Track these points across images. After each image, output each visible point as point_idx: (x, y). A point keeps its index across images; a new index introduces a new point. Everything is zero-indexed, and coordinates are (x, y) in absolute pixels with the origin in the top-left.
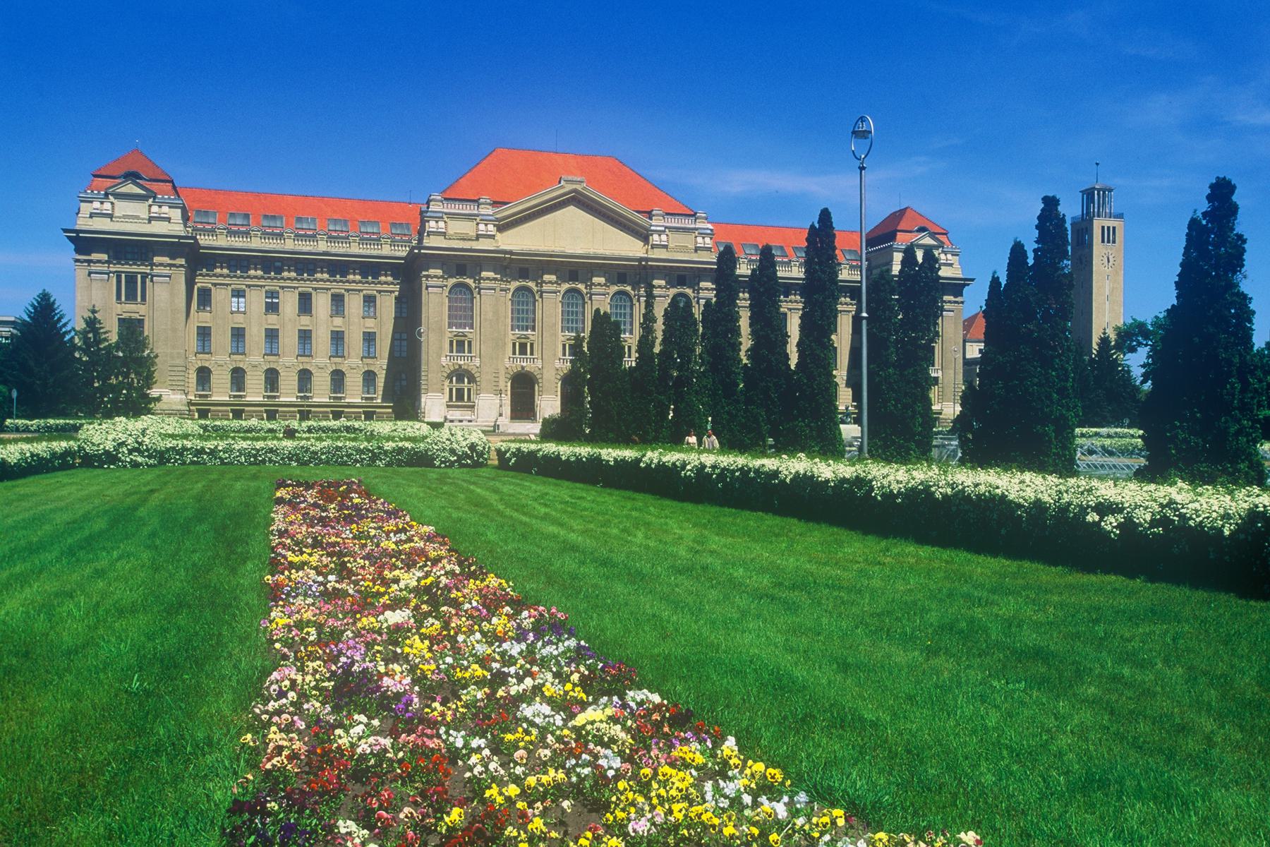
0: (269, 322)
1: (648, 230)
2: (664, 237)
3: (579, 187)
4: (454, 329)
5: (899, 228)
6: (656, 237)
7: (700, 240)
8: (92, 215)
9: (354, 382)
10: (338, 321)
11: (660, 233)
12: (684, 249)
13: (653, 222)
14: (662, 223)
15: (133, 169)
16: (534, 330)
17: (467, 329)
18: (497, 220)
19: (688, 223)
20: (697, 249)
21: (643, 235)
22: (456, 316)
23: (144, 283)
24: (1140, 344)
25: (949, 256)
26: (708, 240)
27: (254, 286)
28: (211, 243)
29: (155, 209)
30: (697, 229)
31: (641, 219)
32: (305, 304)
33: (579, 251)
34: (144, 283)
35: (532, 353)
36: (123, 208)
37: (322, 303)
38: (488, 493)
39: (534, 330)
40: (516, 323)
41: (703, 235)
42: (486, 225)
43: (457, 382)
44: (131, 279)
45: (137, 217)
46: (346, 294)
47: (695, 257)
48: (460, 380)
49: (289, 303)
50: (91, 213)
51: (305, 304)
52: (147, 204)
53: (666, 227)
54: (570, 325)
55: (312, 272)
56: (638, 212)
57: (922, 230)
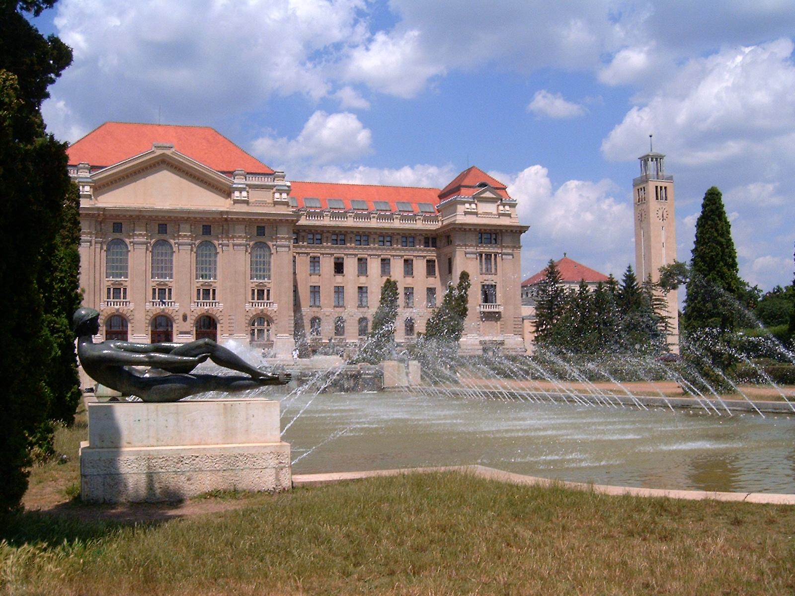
0: (313, 281)
1: (231, 187)
2: (244, 194)
3: (168, 152)
4: (111, 278)
5: (463, 184)
6: (237, 194)
7: (277, 195)
8: (466, 213)
9: (352, 328)
10: (363, 279)
11: (241, 190)
12: (263, 204)
13: (236, 181)
14: (243, 181)
15: (483, 181)
16: (269, 279)
17: (168, 279)
18: (94, 182)
19: (267, 181)
20: (500, 215)
21: (227, 192)
22: (113, 267)
23: (495, 259)
24: (680, 282)
25: (507, 208)
26: (284, 195)
27: (350, 254)
28: (384, 225)
29: (501, 208)
30: (275, 186)
31: (224, 179)
32: (339, 268)
33: (167, 206)
34: (495, 259)
35: (268, 299)
36: (483, 208)
37: (351, 265)
38: (413, 418)
39: (215, 278)
40: (254, 273)
41: (281, 192)
42: (281, 194)
43: (258, 325)
44: (488, 256)
45: (491, 214)
46: (414, 259)
47: (273, 210)
48: (260, 324)
49: (327, 265)
50: (465, 212)
51: (339, 268)
52: (496, 204)
53: (247, 185)
54: (204, 273)
55: (344, 242)
56: (222, 172)
57: (483, 185)
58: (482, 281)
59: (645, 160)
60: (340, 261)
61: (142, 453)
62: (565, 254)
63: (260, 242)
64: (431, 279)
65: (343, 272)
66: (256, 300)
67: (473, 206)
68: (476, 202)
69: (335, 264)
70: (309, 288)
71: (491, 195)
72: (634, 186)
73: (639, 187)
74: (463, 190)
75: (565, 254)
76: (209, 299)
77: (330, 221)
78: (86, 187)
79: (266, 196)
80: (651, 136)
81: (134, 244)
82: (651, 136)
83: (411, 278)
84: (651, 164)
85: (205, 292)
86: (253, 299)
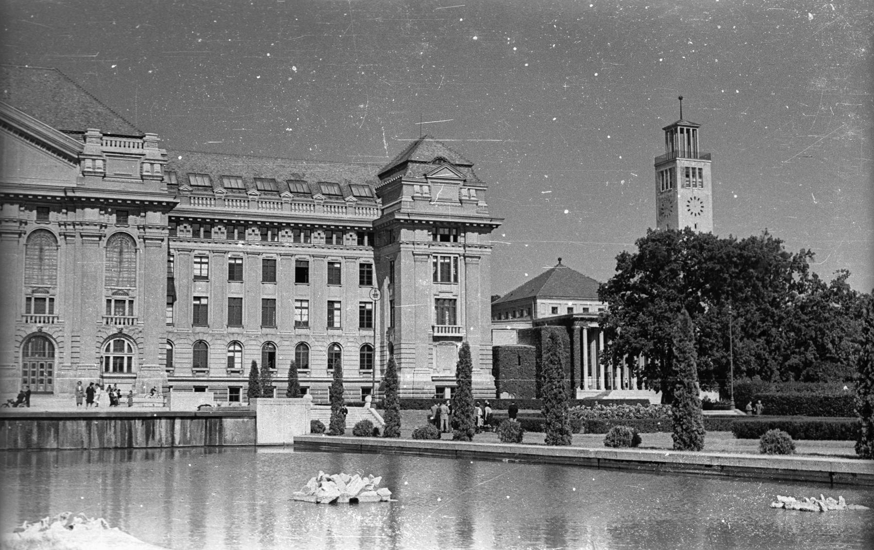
6: (88, 163)
32: (302, 275)
45: (450, 200)
51: (302, 275)
58: (437, 293)
59: (671, 130)
60: (302, 266)
61: (825, 426)
62: (560, 259)
63: (121, 233)
64: (366, 289)
65: (307, 282)
66: (32, 313)
67: (426, 188)
68: (430, 184)
69: (297, 269)
70: (261, 301)
71: (449, 174)
72: (657, 166)
73: (663, 169)
74: (410, 165)
75: (560, 259)
76: (44, 313)
77: (292, 209)
78: (97, 161)
79: (134, 168)
80: (680, 98)
81: (145, 239)
82: (680, 98)
83: (338, 288)
84: (680, 138)
85: (265, 302)
86: (109, 312)
